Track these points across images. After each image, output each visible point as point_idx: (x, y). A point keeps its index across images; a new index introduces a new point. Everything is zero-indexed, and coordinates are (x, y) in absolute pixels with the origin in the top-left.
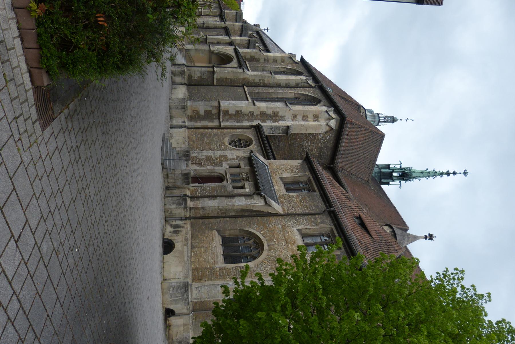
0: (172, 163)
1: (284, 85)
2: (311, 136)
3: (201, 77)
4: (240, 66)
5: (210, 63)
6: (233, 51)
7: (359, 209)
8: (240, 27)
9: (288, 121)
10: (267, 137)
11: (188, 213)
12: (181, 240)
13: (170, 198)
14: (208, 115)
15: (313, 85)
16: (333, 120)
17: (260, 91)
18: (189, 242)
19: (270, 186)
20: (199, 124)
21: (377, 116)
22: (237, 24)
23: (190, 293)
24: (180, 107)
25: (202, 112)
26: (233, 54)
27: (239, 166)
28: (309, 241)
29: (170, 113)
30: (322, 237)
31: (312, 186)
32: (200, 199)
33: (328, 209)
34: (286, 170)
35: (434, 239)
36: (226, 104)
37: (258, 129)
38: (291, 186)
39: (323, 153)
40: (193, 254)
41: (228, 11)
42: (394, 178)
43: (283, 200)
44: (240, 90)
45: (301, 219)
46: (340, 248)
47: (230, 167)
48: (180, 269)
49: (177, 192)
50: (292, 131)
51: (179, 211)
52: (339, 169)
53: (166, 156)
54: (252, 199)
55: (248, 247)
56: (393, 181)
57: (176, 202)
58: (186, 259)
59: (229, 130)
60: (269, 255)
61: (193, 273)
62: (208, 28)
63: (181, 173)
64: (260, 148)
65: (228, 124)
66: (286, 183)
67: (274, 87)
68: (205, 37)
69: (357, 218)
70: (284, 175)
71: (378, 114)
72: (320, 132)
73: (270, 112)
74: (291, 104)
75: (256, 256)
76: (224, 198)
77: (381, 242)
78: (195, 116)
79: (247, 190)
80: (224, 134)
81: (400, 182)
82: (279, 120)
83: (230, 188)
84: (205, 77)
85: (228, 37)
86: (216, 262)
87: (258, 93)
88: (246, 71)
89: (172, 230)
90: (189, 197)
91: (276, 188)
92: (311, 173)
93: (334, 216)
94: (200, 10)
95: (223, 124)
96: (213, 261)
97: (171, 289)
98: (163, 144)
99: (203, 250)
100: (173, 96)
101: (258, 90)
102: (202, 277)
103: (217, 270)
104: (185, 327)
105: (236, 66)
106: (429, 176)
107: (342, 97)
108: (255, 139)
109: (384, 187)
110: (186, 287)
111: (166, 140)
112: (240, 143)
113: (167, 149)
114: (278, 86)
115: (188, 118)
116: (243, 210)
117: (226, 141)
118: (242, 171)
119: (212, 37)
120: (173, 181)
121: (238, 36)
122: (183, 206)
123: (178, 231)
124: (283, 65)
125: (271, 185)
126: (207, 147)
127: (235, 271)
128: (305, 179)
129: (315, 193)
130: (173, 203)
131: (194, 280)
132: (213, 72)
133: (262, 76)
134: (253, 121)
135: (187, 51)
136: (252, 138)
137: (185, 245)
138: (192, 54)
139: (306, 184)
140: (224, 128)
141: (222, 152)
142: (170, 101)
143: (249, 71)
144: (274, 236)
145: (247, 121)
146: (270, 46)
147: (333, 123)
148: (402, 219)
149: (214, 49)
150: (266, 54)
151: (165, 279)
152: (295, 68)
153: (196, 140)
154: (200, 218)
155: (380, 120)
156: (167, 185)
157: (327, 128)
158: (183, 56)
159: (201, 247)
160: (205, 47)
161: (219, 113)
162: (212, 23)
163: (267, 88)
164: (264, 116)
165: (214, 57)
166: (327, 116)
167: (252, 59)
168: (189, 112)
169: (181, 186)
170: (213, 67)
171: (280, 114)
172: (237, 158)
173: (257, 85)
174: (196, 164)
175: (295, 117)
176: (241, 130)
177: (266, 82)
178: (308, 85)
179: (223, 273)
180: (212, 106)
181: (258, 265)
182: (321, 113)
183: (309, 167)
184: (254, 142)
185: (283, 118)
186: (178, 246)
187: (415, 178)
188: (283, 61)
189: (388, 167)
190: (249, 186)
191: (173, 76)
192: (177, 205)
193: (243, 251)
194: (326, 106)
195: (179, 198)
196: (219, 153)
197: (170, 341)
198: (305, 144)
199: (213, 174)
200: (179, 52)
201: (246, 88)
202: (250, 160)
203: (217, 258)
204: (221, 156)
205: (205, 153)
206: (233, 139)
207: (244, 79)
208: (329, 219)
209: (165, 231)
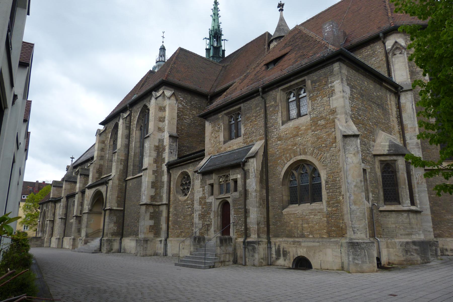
0: (208, 256)
1: (127, 140)
2: (180, 115)
3: (115, 223)
4: (105, 183)
5: (101, 213)
6: (90, 190)
7: (257, 66)
8: (67, 183)
9: (164, 136)
10: (179, 158)
11: (263, 240)
12: (294, 249)
13: (247, 259)
14: (155, 216)
15: (128, 113)
16: (165, 93)
17: (132, 164)
18: (297, 240)
19: (233, 153)
20: (164, 226)
21: (158, 63)
22: (64, 186)
23: (360, 241)
24: (145, 246)
25: (151, 223)
26: (93, 191)
27: (212, 185)
28: (293, 113)
29: (151, 256)
30: (290, 101)
31: (234, 111)
32: (248, 226)
33: (261, 94)
34: (216, 138)
35: (282, 3)
36: (144, 197)
37: (171, 166)
38: (233, 133)
39: (197, 105)
40: (311, 236)
41: (51, 194)
42: (219, 45)
43: (248, 140)
44: (130, 184)
45: (270, 122)
46: (304, 81)
47: (212, 194)
48: (329, 252)
49: (240, 252)
50: (175, 133)
51: (262, 250)
52: (212, 91)
53: (201, 263)
54: (249, 172)
55: (301, 176)
56: (222, 46)
57: (251, 253)
58: (318, 244)
59: (171, 196)
60: (312, 154)
61: (333, 237)
62: (66, 215)
63: (220, 247)
64: (191, 164)
65: (165, 196)
66: (230, 138)
67: (128, 150)
68: (75, 218)
69: (268, 68)
70: (222, 139)
71: (157, 62)
72: (177, 105)
73: (154, 154)
74: (147, 133)
75: (312, 168)
76: (248, 201)
77: (291, 45)
78: (155, 230)
79: (239, 176)
80: (176, 200)
81: (222, 40)
82: (163, 145)
83: (236, 194)
84: (115, 218)
85: (76, 195)
86: (320, 211)
87: (134, 166)
88: (111, 178)
89: (282, 258)
90: (246, 239)
91: (235, 147)
92: (220, 112)
93: (268, 88)
94: (48, 221)
95: (165, 201)
96: (319, 214)
97: (357, 262)
98: (187, 266)
99: (306, 225)
100: (133, 251)
101: (132, 166)
102: (338, 227)
103: (329, 209)
104: (390, 246)
105: (105, 187)
106: (218, 14)
107: (142, 86)
108: (182, 169)
109: (226, 55)
110: (353, 245)
111: (183, 263)
112: (185, 184)
113: (192, 262)
114: (128, 146)
115: (157, 237)
116: (261, 181)
117: (182, 198)
118: (217, 181)
119: (75, 211)
120: (228, 255)
121: (76, 185)
122: (256, 246)
123: (284, 251)
124: (108, 142)
125: (232, 153)
126: (188, 218)
127: (331, 190)
128: (226, 118)
129: (242, 108)
130: (253, 256)
131: (342, 235)
132: (111, 210)
133: (117, 161)
134: (163, 171)
135: (87, 236)
136: (180, 172)
137: (300, 245)
138: (90, 231)
139: (232, 117)
140: (169, 201)
141: (195, 202)
142: (138, 255)
143: (111, 175)
144: (290, 149)
145: (163, 177)
146: (88, 156)
147: (168, 93)
148: (258, 38)
149: (87, 209)
150: (95, 159)
151: (342, 268)
152: (110, 130)
153: (180, 229)
154: (270, 227)
155: (162, 61)
156: (231, 263)
157: (173, 98)
158: (92, 240)
159: (302, 227)
160: (85, 218)
161: (153, 205)
162: (61, 210)
163: (129, 157)
164: (158, 160)
165: (96, 209)
166: (160, 98)
167: (99, 171)
168: (151, 236)
169: (233, 247)
170: (105, 210)
171: (157, 144)
172: (203, 187)
173: (126, 167)
174: (208, 230)
175: (160, 130)
176: (172, 183)
177: (123, 158)
178: (128, 118)
179: (333, 204)
180: (146, 212)
181: (324, 166)
182: (158, 104)
183: (214, 115)
184: (184, 170)
185: (161, 141)
186: (301, 252)
187: (219, 26)
188: (103, 142)
189: (208, 50)
190: (234, 174)
191: (112, 251)
192: (254, 252)
193: (307, 181)
194: (151, 99)
195: (247, 250)
196: (197, 206)
197: (405, 263)
198: (187, 121)
199: (220, 213)
200: (88, 244)
201: (128, 178)
202: (206, 173)
203: (316, 210)
204: (200, 203)
205: (196, 220)
206: (181, 192)
207: (119, 180)
208: (271, 93)
209: (284, 266)
